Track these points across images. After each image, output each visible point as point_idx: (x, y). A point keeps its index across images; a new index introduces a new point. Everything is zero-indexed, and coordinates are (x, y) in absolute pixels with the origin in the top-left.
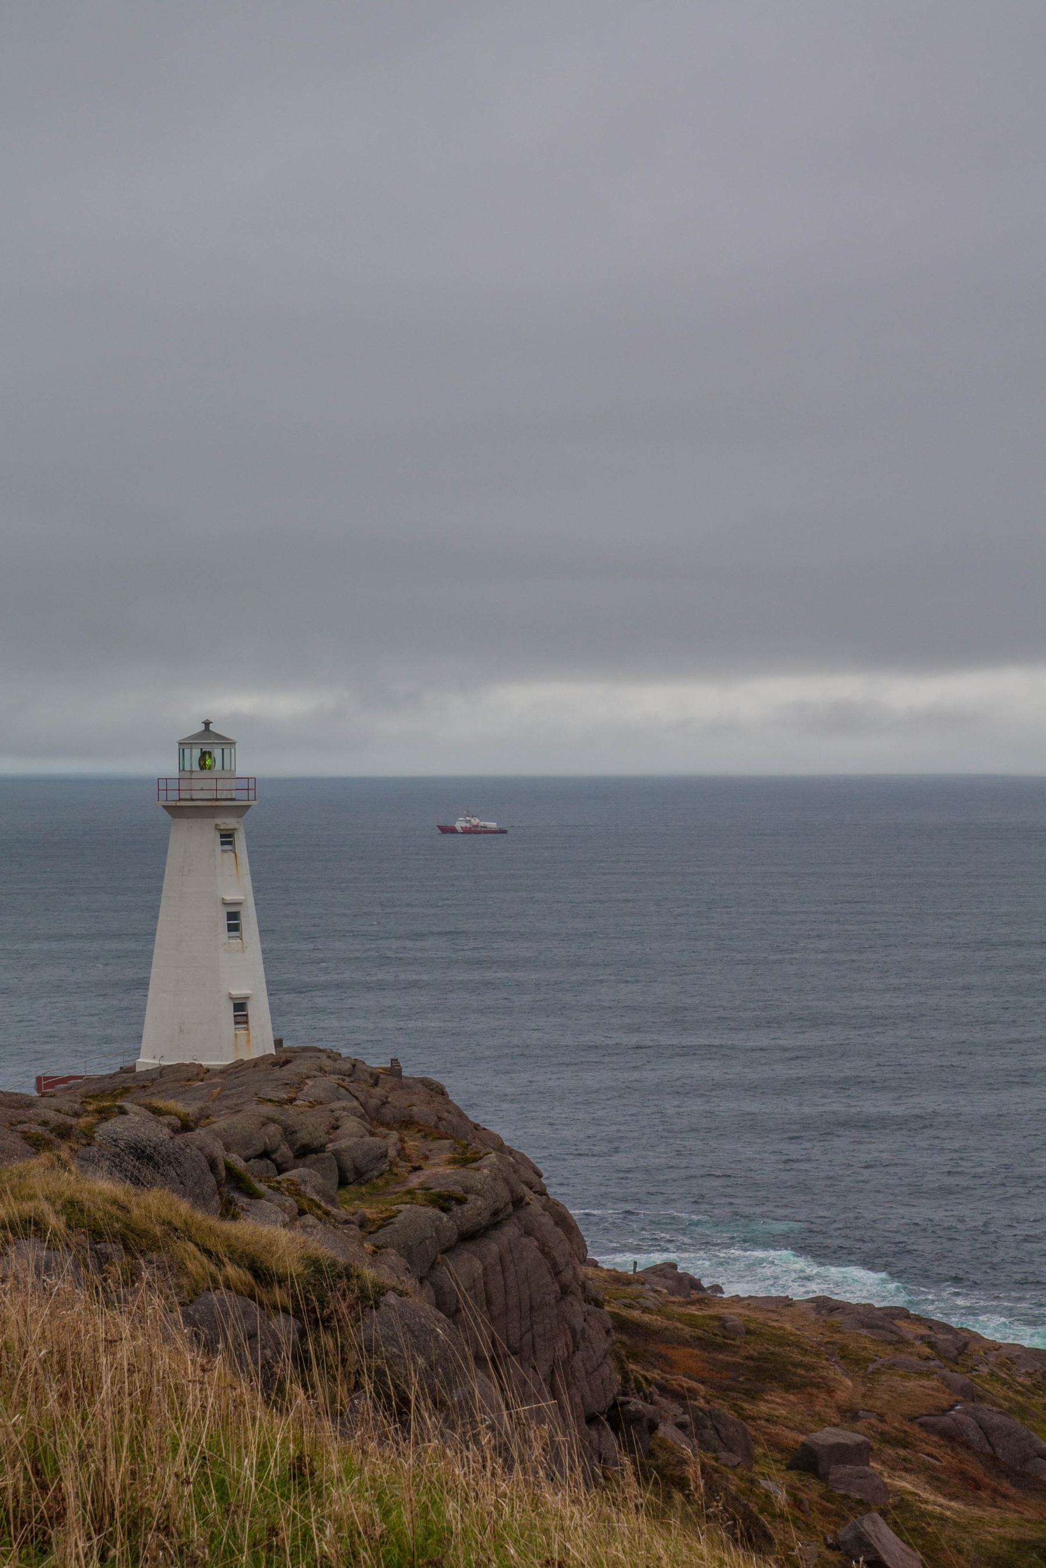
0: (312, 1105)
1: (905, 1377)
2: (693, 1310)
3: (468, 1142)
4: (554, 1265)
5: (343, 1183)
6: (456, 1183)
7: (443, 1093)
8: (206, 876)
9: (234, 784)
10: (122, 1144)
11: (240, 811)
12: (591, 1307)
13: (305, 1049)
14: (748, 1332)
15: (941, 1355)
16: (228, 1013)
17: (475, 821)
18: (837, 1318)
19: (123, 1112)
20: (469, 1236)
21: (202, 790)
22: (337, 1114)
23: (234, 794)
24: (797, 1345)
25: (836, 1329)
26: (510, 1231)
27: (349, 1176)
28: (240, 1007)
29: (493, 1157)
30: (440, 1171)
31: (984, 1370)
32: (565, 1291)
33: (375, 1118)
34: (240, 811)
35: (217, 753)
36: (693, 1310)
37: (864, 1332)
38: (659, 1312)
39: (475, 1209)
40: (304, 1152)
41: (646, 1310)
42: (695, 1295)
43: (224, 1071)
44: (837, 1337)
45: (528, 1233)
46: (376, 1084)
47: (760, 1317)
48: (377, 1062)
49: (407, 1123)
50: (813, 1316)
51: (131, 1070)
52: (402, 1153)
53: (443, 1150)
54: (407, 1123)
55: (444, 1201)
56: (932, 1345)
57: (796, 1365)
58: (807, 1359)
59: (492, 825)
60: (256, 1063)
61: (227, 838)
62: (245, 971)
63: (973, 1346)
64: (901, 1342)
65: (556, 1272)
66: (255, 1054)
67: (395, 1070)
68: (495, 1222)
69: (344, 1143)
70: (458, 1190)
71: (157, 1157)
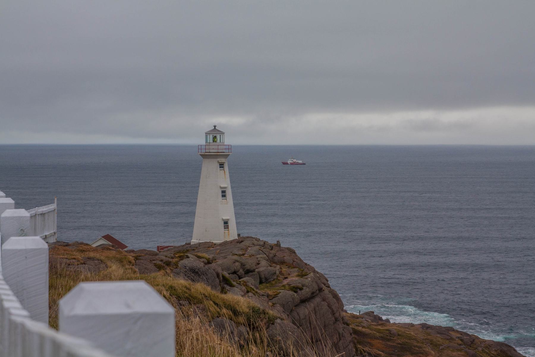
0: (250, 256)
1: (453, 351)
2: (379, 327)
3: (304, 270)
4: (333, 311)
5: (261, 282)
6: (299, 283)
7: (295, 253)
8: (214, 179)
9: (224, 147)
10: (187, 268)
11: (226, 156)
12: (345, 326)
13: (248, 237)
14: (399, 335)
15: (465, 344)
16: (222, 224)
17: (295, 160)
18: (429, 331)
19: (188, 257)
20: (303, 301)
21: (213, 149)
22: (259, 259)
23: (224, 151)
24: (415, 339)
25: (429, 334)
26: (318, 300)
27: (263, 280)
28: (226, 223)
29: (312, 274)
30: (294, 279)
31: (480, 349)
32: (336, 320)
33: (272, 261)
34: (226, 156)
35: (218, 137)
36: (379, 327)
37: (439, 335)
38: (368, 328)
39: (306, 292)
40: (248, 272)
41: (363, 327)
42: (380, 322)
43: (221, 245)
44: (429, 337)
45: (324, 300)
46: (272, 249)
47: (403, 330)
48: (272, 241)
49: (282, 263)
50: (421, 330)
51: (189, 244)
52: (281, 273)
53: (295, 272)
54: (282, 263)
55: (295, 289)
56: (462, 340)
57: (415, 346)
58: (418, 344)
59: (300, 162)
60: (231, 242)
61: (222, 165)
62: (227, 210)
63: (476, 341)
64: (451, 339)
65: (333, 313)
66: (231, 239)
67: (278, 245)
68: (313, 296)
69: (261, 269)
70: (300, 285)
71: (199, 273)
